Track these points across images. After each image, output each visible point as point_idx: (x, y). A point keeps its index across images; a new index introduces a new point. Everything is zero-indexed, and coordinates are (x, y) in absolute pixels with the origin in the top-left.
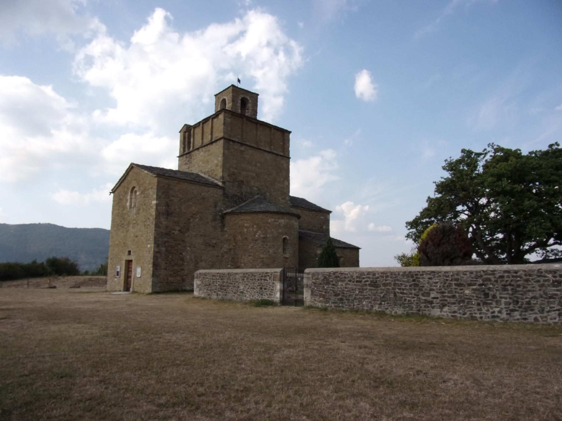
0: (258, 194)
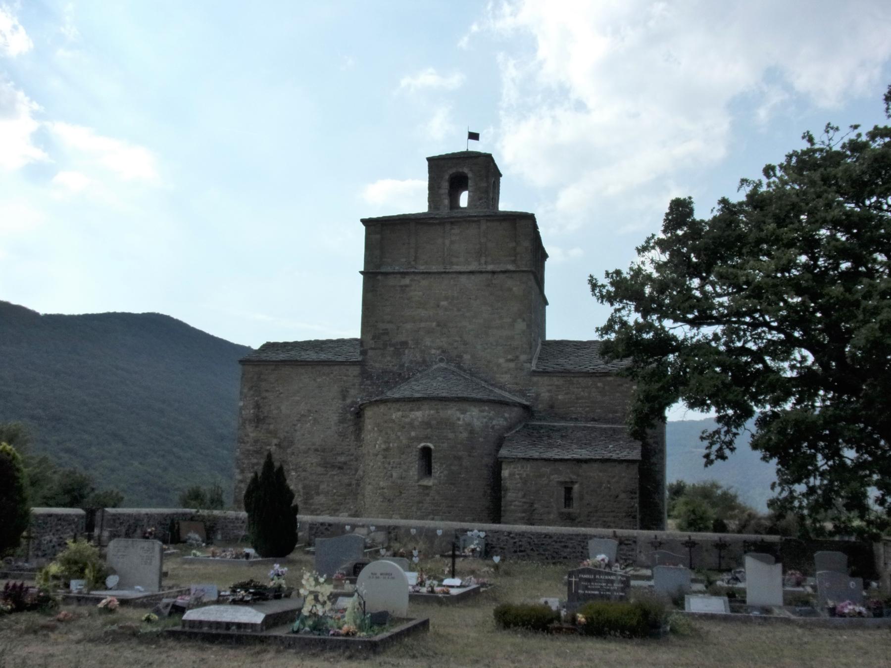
0: (441, 360)
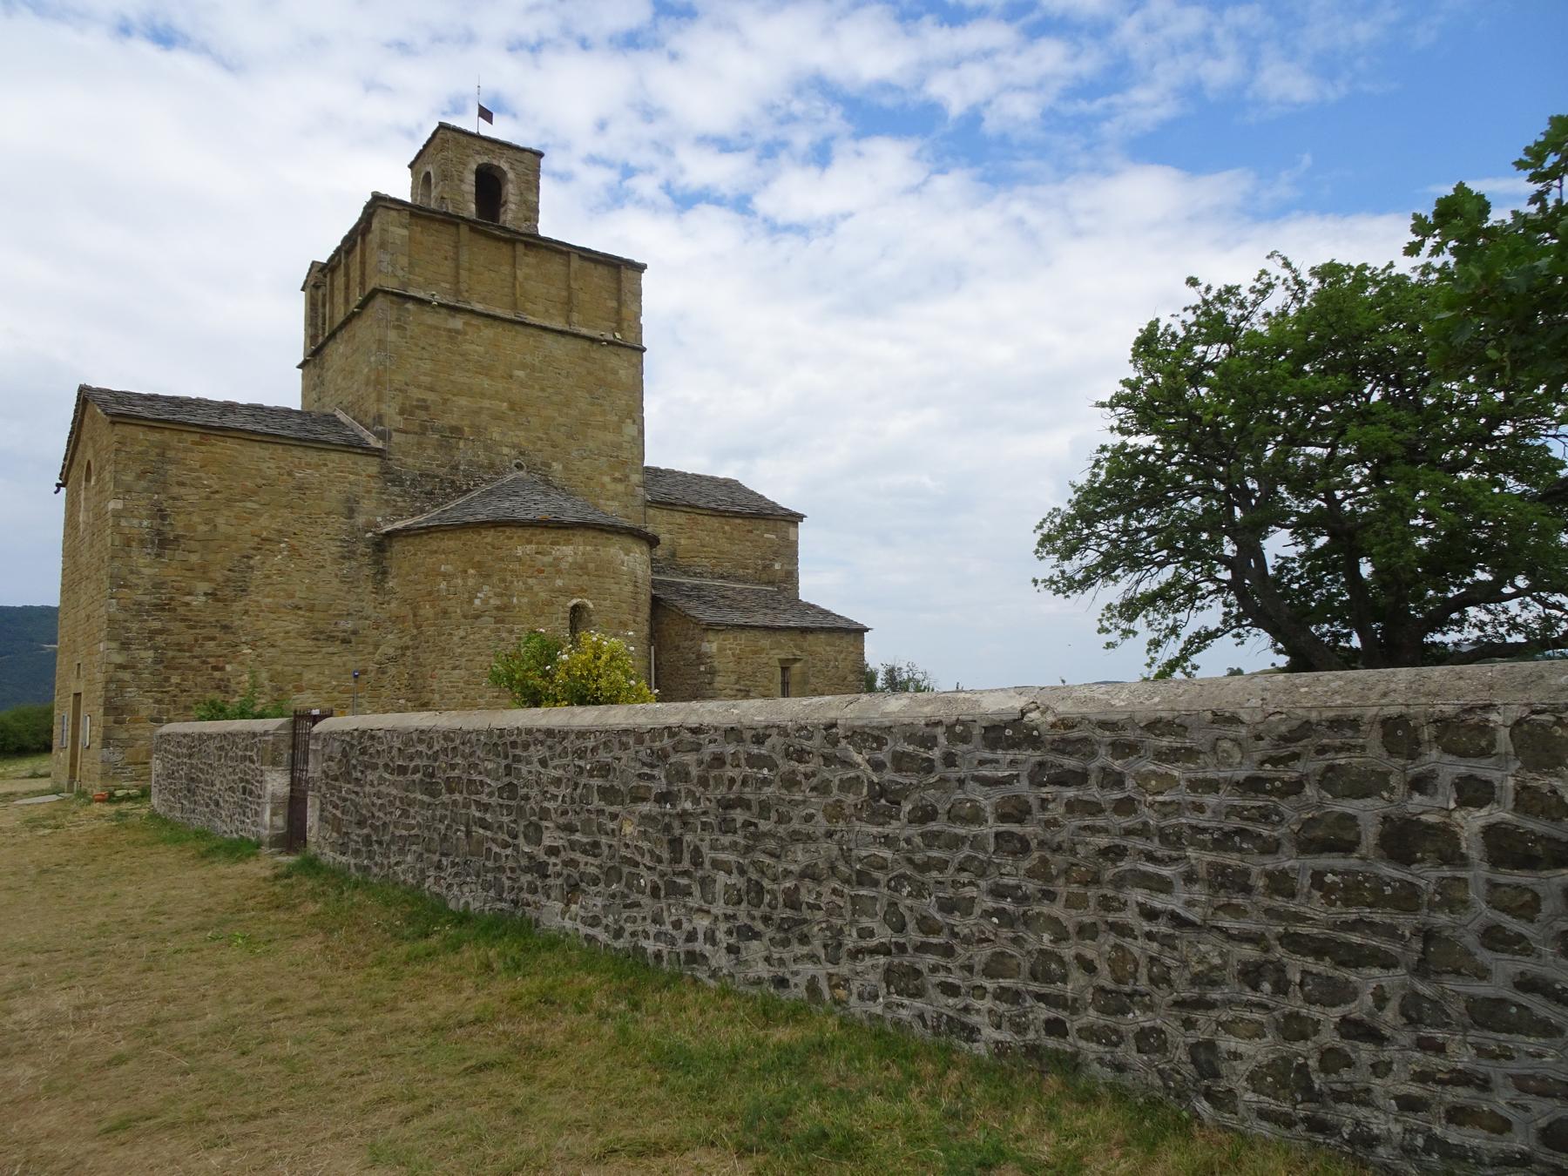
0: (519, 466)
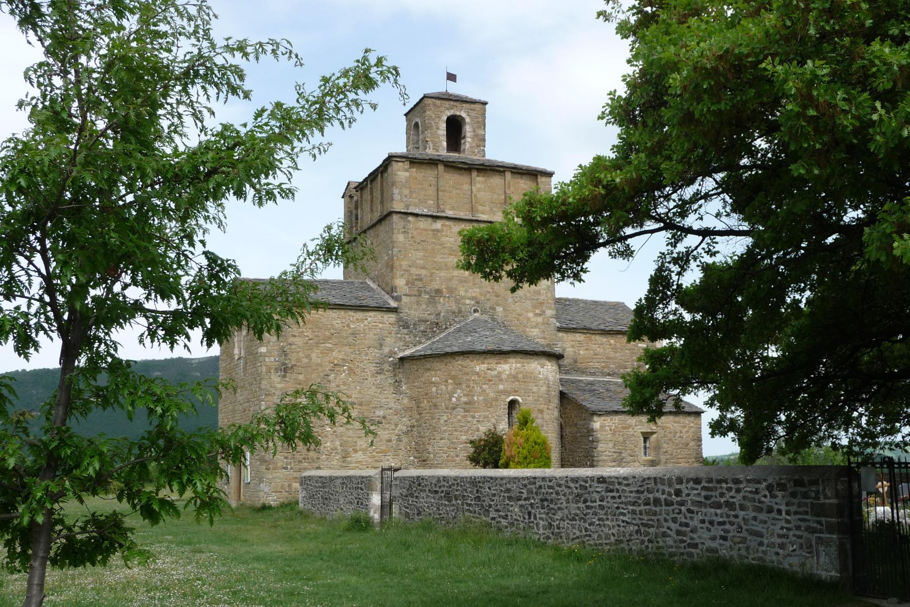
0: (475, 311)
